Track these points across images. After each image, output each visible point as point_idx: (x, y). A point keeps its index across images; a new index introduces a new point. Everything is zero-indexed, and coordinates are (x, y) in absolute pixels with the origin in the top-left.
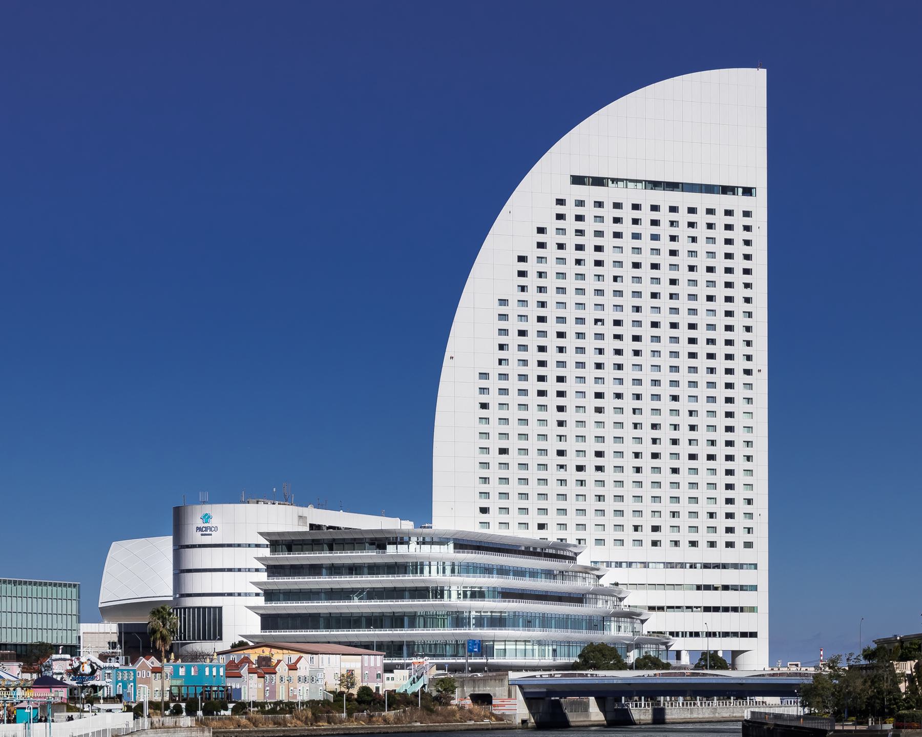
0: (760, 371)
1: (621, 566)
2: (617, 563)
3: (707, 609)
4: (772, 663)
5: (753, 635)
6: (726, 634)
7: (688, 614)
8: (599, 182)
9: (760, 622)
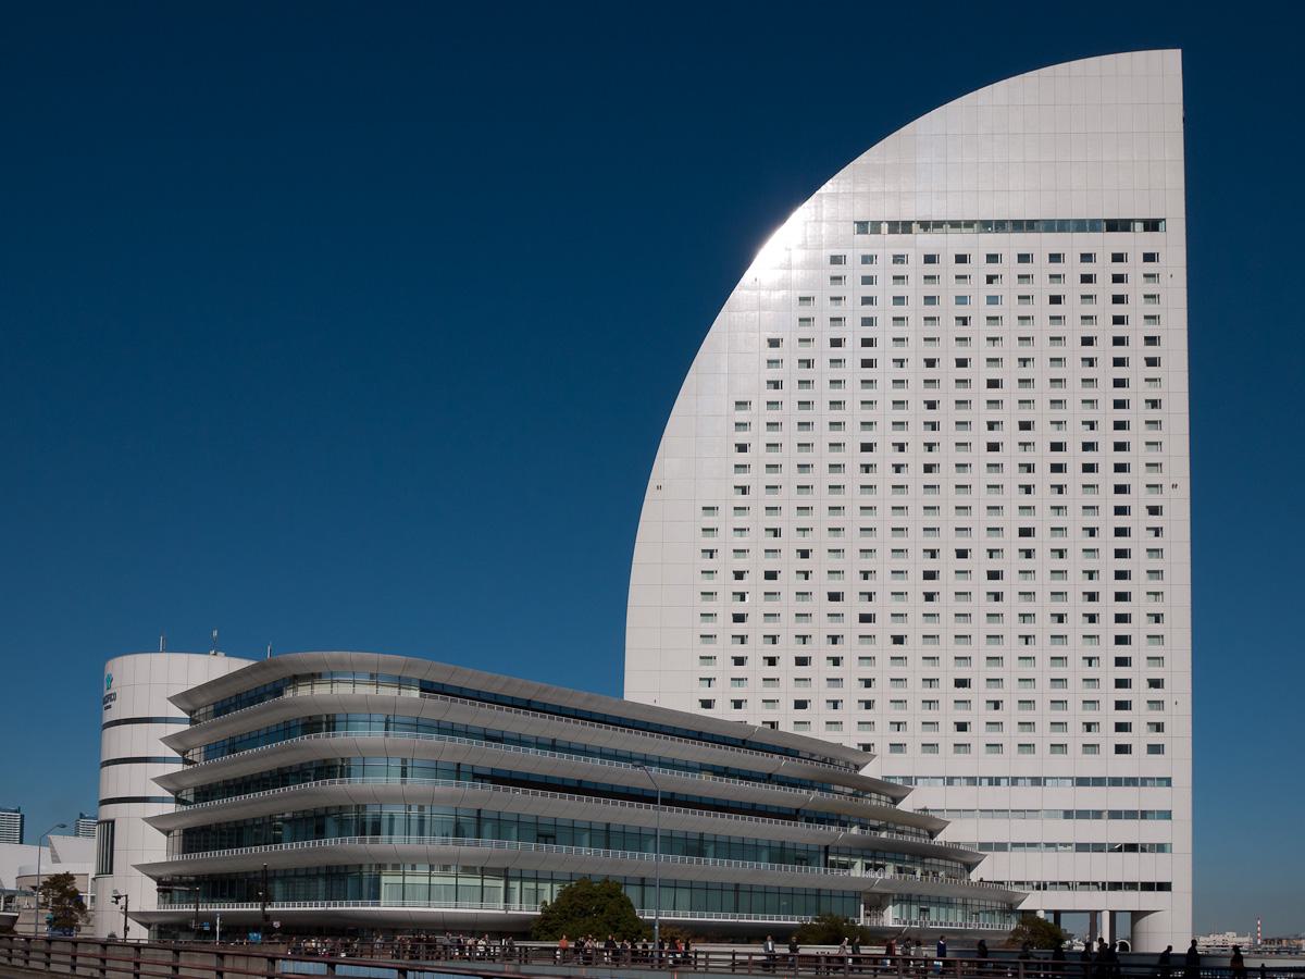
0: (1175, 486)
1: (998, 784)
2: (990, 779)
3: (1082, 847)
4: (1200, 922)
5: (1164, 887)
6: (1116, 886)
7: (1050, 855)
8: (905, 227)
9: (1177, 867)
